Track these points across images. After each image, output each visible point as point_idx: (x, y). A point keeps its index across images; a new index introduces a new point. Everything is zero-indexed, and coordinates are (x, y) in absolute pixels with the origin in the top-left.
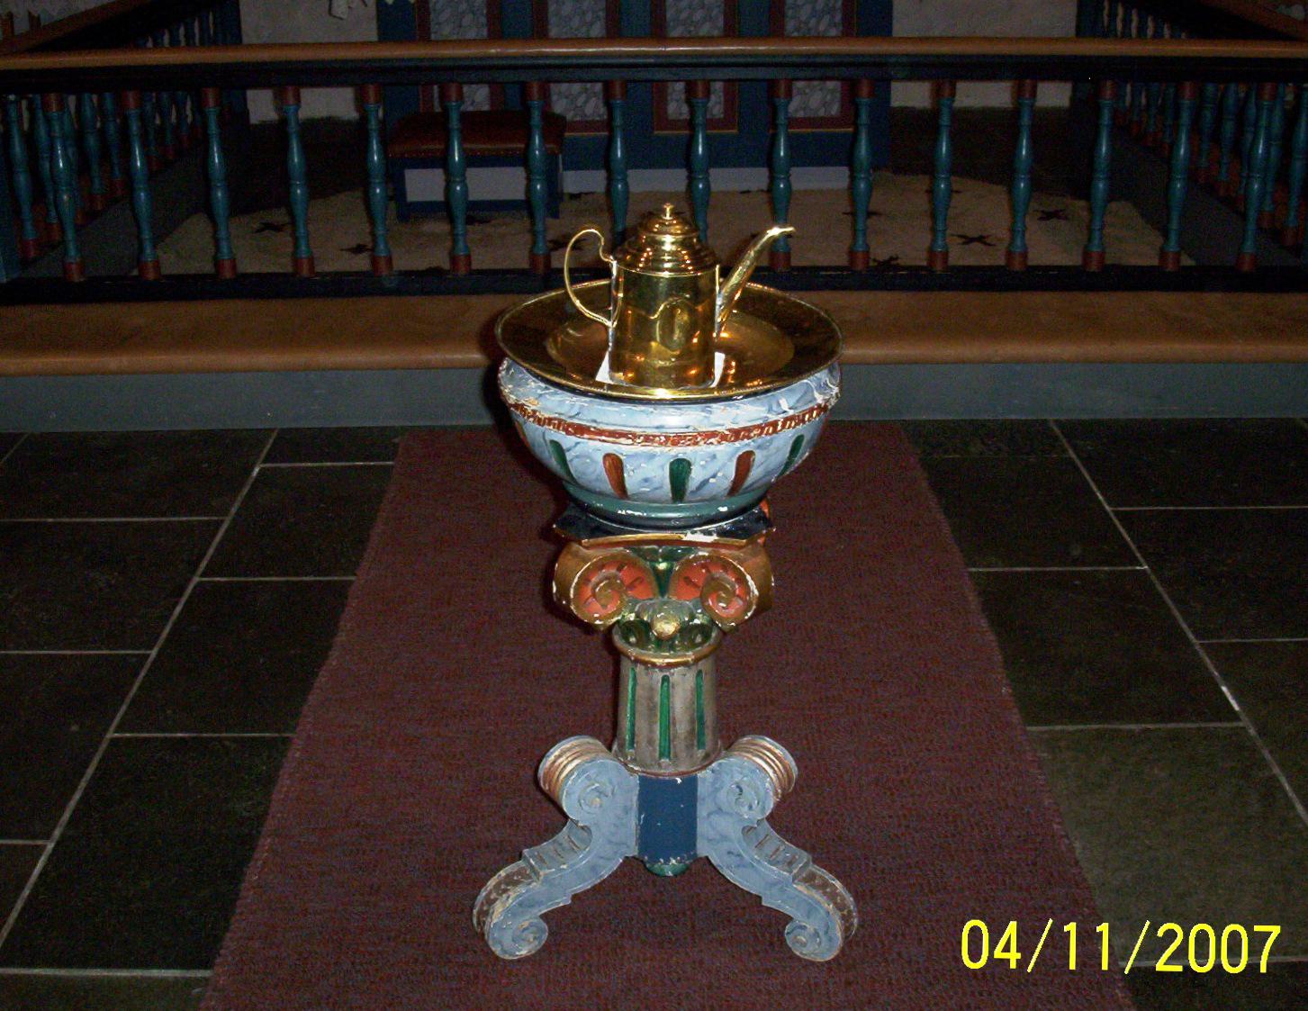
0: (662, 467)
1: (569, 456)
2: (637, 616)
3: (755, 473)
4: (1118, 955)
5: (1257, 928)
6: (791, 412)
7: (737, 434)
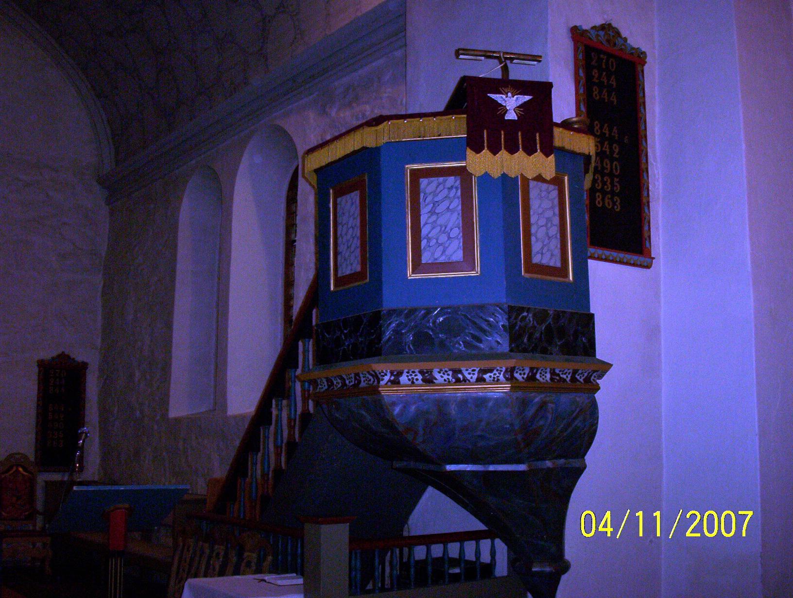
4: (666, 530)
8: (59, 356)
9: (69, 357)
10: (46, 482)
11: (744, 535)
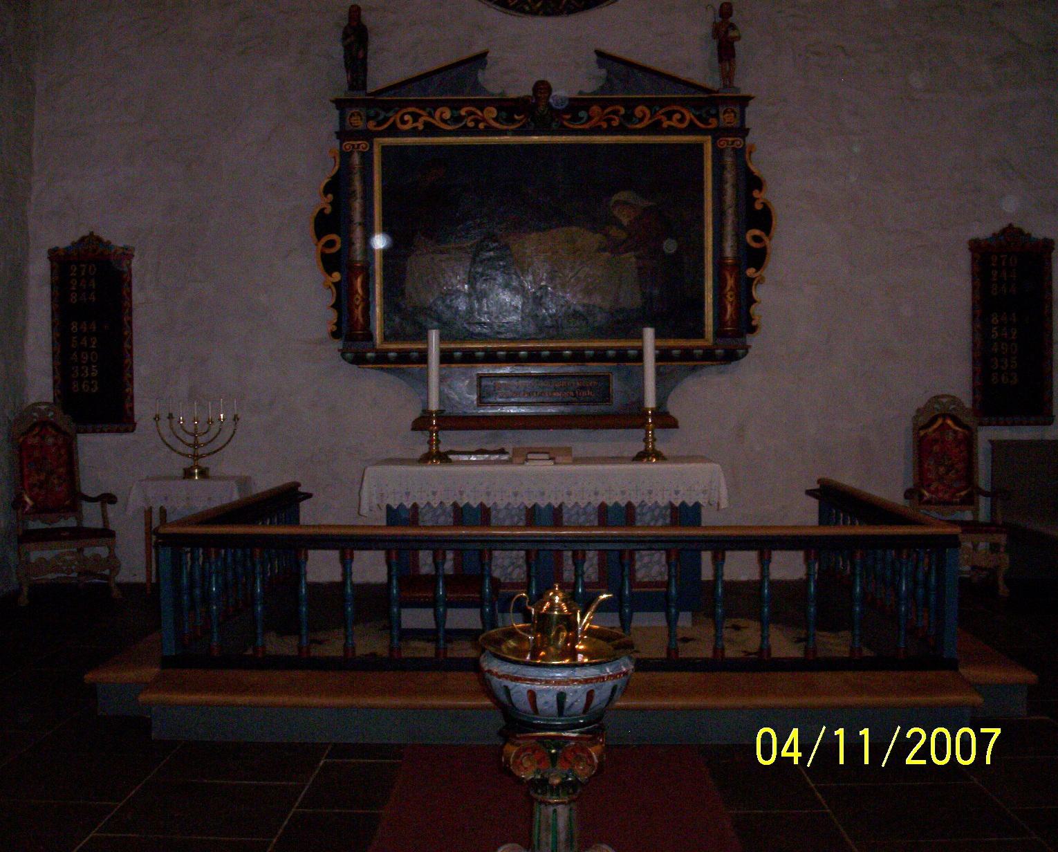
0: (553, 696)
1: (512, 692)
2: (542, 776)
3: (596, 701)
4: (877, 752)
5: (983, 730)
6: (611, 673)
7: (586, 681)
8: (1004, 231)
9: (1020, 231)
10: (991, 442)
11: (988, 762)
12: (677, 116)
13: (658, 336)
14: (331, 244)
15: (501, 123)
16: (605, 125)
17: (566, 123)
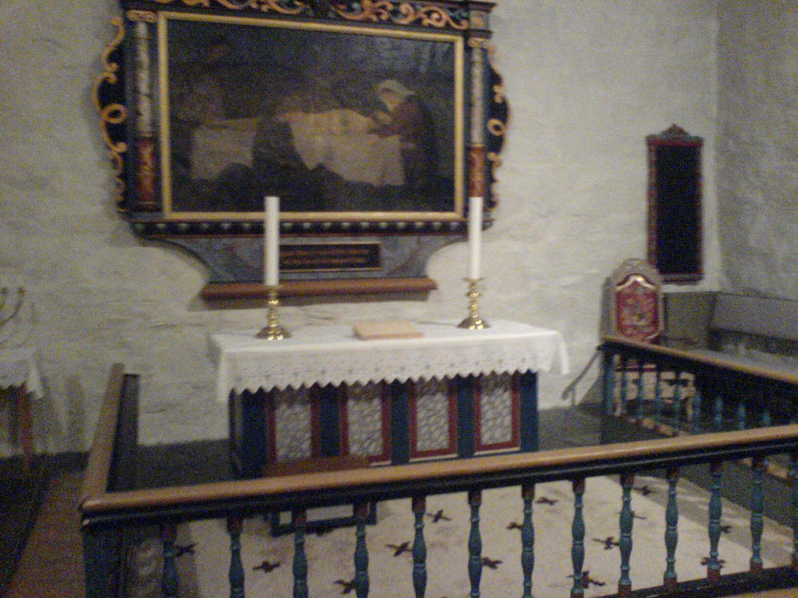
12: (435, 16)
13: (283, 208)
14: (115, 114)
15: (282, 7)
16: (375, 18)
17: (342, 14)
